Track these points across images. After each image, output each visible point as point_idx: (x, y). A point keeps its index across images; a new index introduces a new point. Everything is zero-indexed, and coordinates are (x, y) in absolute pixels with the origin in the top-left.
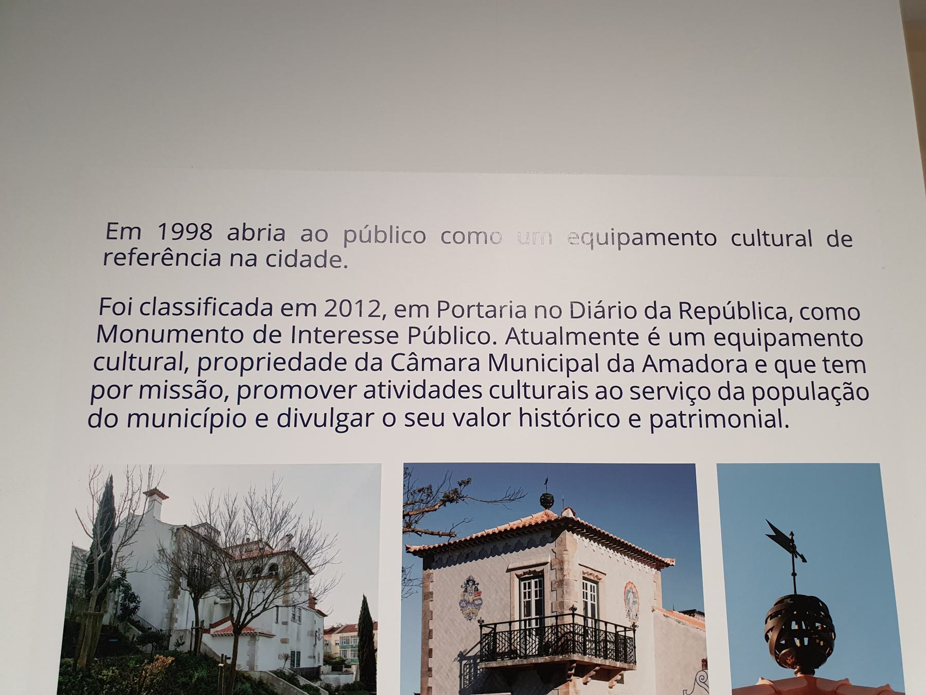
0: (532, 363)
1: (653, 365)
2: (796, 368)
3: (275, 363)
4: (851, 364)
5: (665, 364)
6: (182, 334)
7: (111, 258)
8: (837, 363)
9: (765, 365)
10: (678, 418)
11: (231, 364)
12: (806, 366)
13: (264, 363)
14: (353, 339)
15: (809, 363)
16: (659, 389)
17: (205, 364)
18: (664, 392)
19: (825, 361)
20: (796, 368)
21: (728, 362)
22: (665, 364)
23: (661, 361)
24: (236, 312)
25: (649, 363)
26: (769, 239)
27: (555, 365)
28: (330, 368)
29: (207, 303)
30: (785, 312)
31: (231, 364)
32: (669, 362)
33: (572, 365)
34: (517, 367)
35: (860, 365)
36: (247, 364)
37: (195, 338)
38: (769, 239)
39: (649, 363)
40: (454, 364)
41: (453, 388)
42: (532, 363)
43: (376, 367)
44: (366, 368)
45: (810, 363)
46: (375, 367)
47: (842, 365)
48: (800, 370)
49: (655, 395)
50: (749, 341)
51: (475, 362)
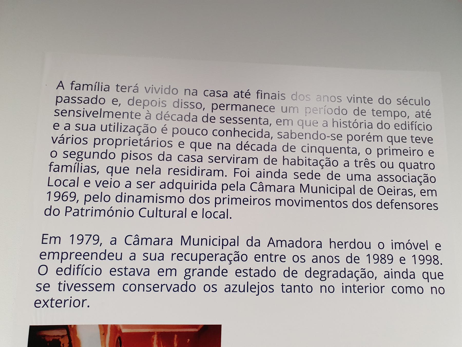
0: (322, 189)
1: (273, 243)
2: (397, 140)
3: (133, 142)
4: (430, 192)
5: (279, 242)
6: (103, 212)
7: (172, 171)
8: (397, 204)
9: (440, 246)
10: (419, 165)
11: (110, 142)
12: (438, 275)
13: (127, 142)
14: (176, 173)
15: (403, 138)
16: (223, 158)
17: (97, 141)
18: (225, 159)
19: (412, 137)
20: (397, 140)
21: (312, 242)
22: (279, 242)
23: (277, 241)
24: (71, 185)
25: (271, 242)
26: (162, 213)
27: (333, 190)
28: (105, 259)
29: (78, 268)
30: (356, 150)
31: (110, 142)
32: (310, 201)
33: (342, 191)
34: (314, 191)
35: (434, 192)
36: (119, 142)
37: (147, 172)
38: (162, 213)
39: (271, 242)
40: (263, 188)
41: (269, 159)
42: (322, 189)
43: (227, 148)
44: (208, 189)
45: (404, 138)
46: (292, 163)
47: (399, 205)
48: (399, 141)
49: (221, 161)
50: (186, 187)
51: (214, 185)
